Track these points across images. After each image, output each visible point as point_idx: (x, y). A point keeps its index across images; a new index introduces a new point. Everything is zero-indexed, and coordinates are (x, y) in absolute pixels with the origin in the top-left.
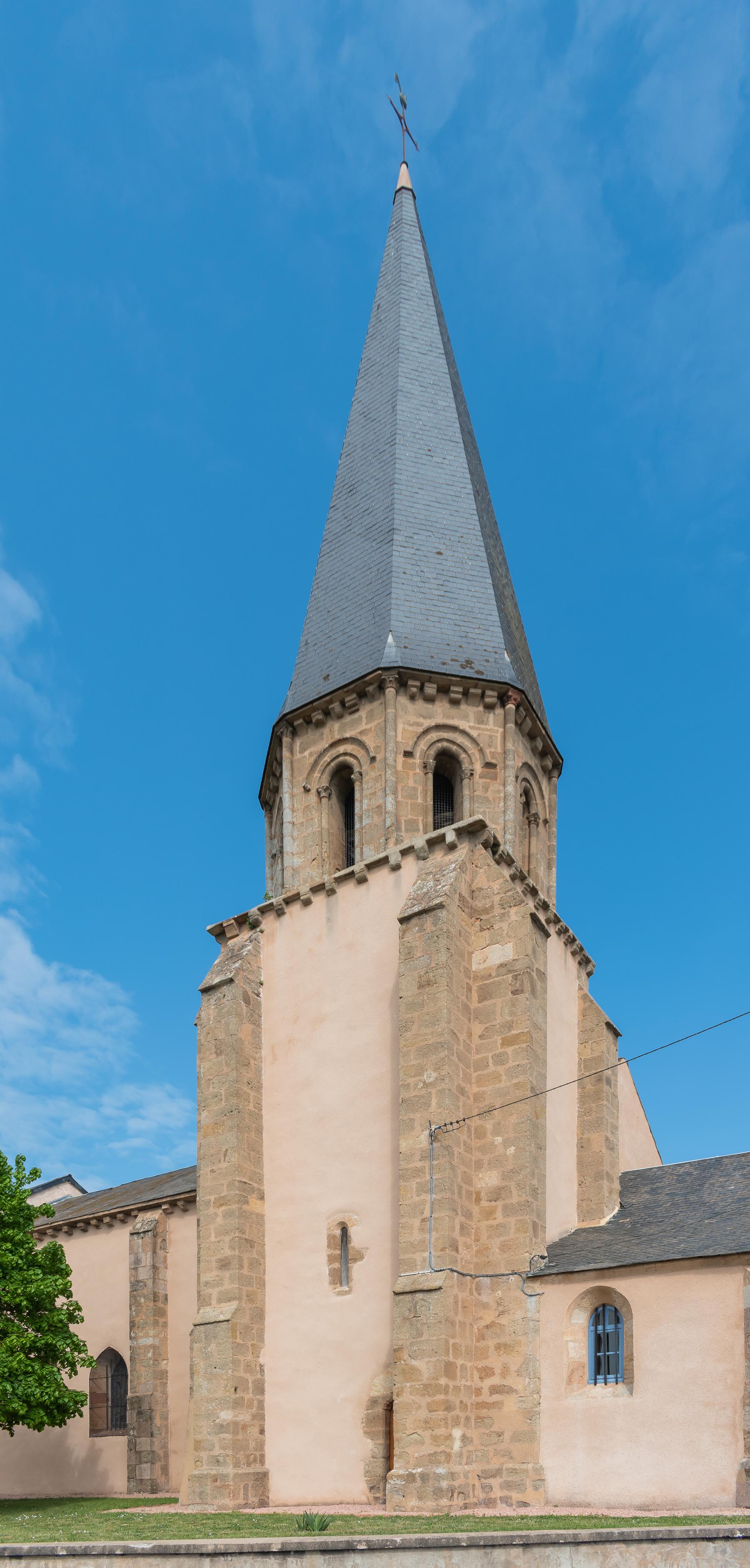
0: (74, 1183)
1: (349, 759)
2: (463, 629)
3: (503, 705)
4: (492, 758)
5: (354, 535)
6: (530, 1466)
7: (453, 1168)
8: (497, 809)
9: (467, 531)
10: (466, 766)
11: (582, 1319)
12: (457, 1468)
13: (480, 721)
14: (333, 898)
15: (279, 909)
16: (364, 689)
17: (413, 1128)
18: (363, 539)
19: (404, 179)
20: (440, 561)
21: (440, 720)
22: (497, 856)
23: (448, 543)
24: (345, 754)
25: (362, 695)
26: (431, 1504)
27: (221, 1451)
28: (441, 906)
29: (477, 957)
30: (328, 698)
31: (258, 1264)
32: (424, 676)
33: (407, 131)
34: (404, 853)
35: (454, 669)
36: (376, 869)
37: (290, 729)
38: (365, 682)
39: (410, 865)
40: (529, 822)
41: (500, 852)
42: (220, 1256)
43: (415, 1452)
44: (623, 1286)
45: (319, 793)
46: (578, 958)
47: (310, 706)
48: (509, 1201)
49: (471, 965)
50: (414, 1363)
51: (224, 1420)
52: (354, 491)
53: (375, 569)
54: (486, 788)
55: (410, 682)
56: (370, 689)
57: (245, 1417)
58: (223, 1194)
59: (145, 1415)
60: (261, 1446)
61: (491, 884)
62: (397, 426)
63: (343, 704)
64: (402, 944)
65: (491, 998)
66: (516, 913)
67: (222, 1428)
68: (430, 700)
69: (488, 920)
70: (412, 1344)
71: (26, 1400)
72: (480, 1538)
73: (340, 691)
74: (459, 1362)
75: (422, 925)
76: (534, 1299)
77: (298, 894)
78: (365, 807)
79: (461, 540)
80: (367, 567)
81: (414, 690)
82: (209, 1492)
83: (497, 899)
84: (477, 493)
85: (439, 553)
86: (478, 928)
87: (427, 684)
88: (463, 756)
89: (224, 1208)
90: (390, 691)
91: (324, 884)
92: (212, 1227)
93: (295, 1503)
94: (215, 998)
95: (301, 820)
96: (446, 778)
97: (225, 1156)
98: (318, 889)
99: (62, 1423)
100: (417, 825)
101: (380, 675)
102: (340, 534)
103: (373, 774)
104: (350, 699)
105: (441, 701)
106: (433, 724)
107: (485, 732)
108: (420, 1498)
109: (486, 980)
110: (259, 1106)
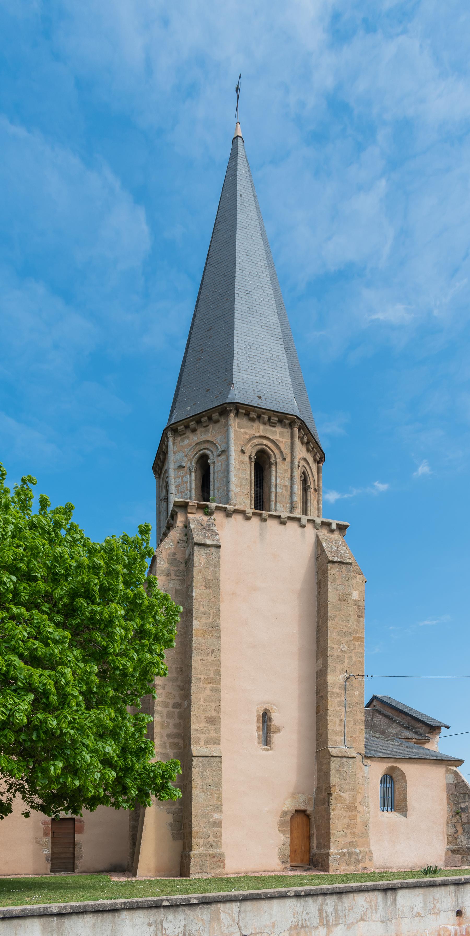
6: (367, 849)
14: (264, 524)
17: (335, 671)
26: (353, 867)
27: (214, 839)
30: (264, 411)
38: (286, 417)
42: (207, 715)
43: (342, 841)
44: (404, 767)
47: (253, 408)
48: (356, 718)
50: (342, 794)
51: (217, 819)
56: (287, 422)
58: (210, 677)
63: (269, 419)
70: (341, 784)
72: (302, 891)
76: (367, 767)
82: (208, 865)
89: (211, 685)
92: (202, 695)
93: (273, 870)
94: (205, 552)
97: (212, 653)
104: (274, 419)
108: (347, 865)
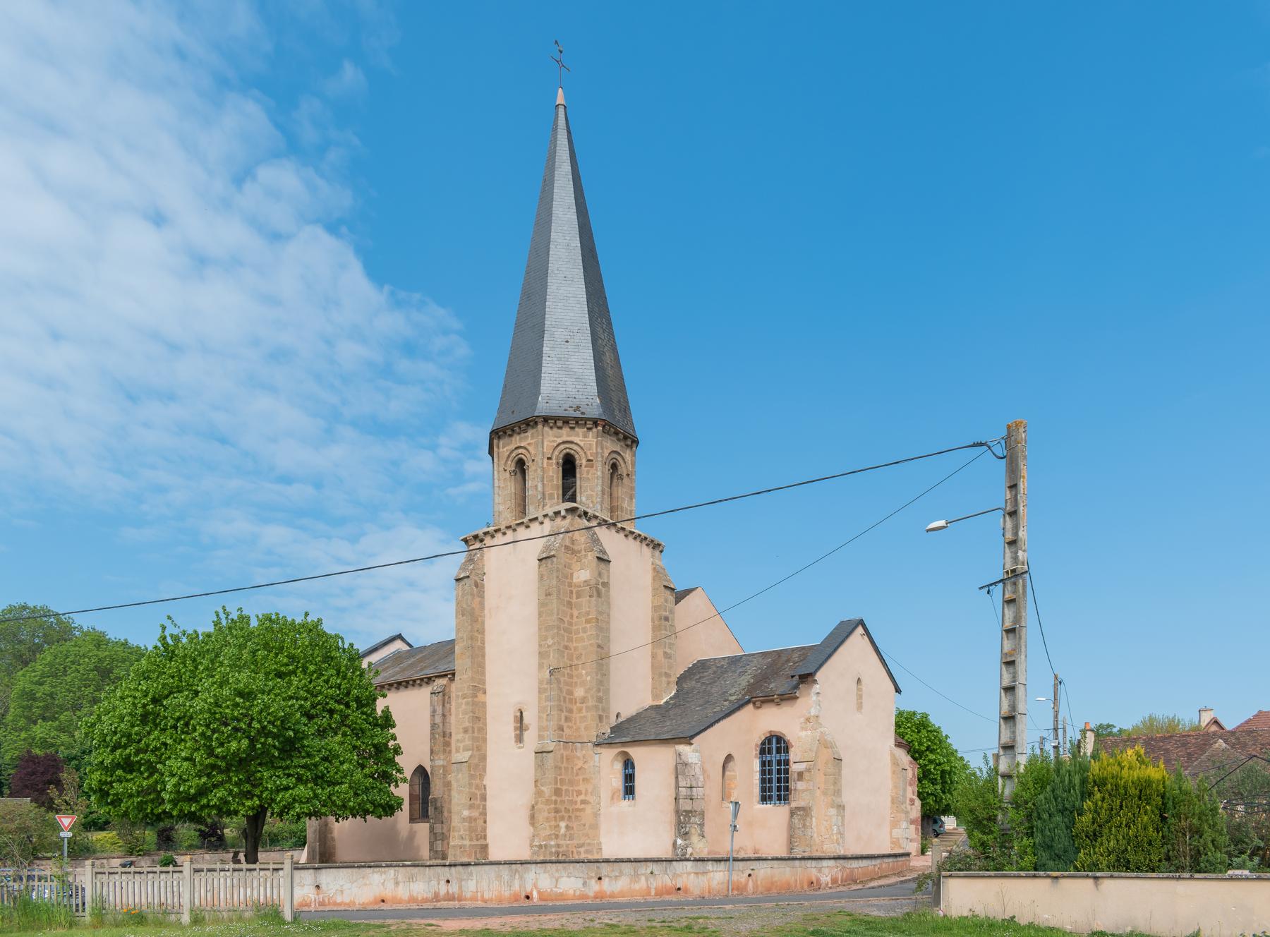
0: (403, 640)
7: (560, 689)
10: (577, 462)
11: (619, 766)
12: (562, 842)
13: (585, 436)
16: (529, 423)
21: (565, 438)
25: (528, 425)
31: (483, 730)
32: (556, 419)
34: (545, 516)
39: (547, 521)
54: (588, 472)
57: (475, 814)
59: (439, 810)
60: (484, 830)
67: (464, 820)
68: (560, 428)
71: (372, 803)
74: (564, 788)
90: (540, 426)
96: (569, 466)
98: (508, 527)
99: (392, 814)
107: (587, 444)
110: (483, 642)
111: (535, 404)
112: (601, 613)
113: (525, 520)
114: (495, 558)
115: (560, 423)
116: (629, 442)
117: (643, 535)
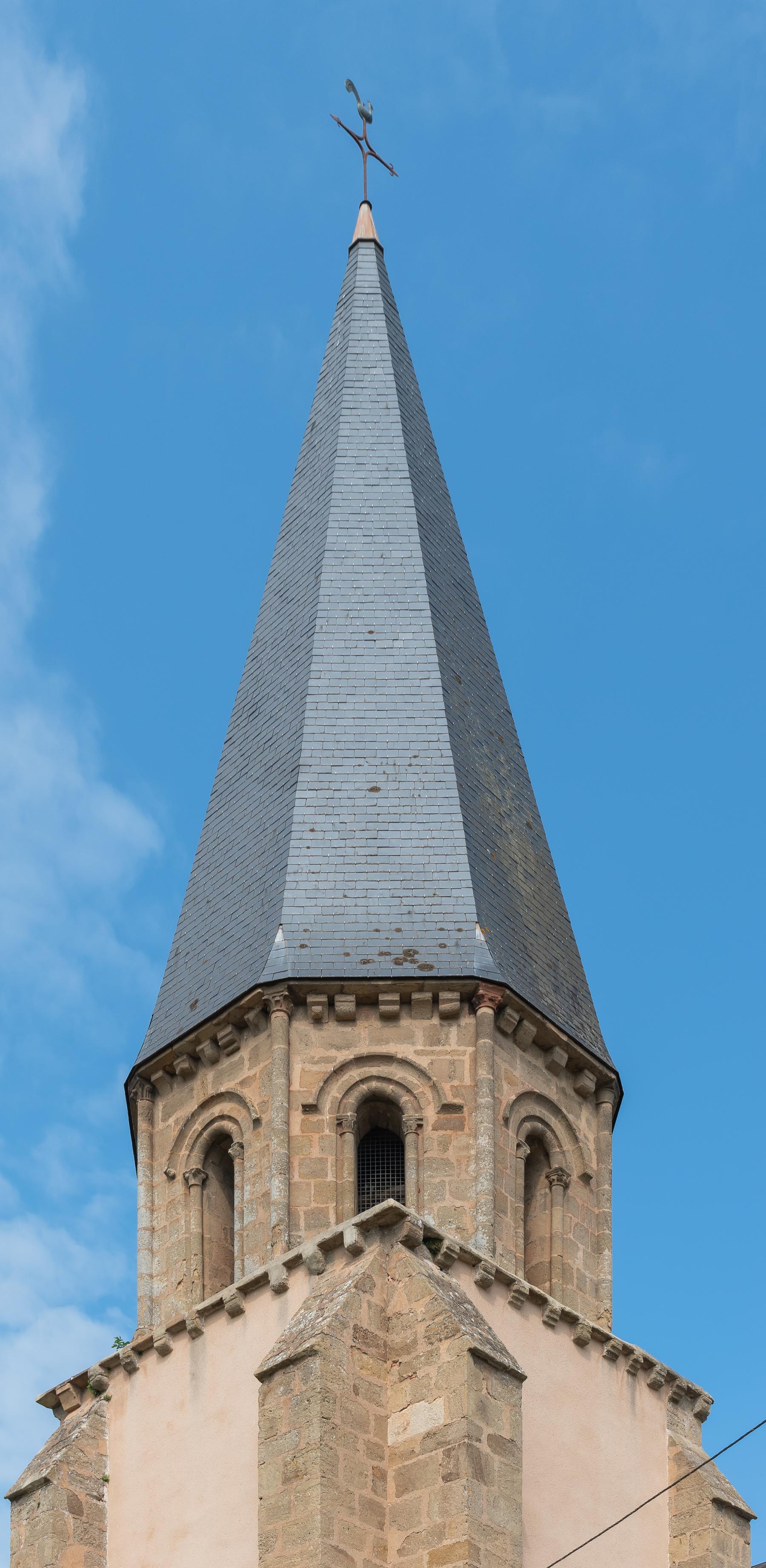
1: (227, 1125)
2: (405, 901)
3: (473, 1011)
4: (455, 1096)
5: (250, 780)
8: (464, 1176)
9: (425, 745)
10: (409, 1115)
14: (199, 1341)
15: (128, 1364)
16: (242, 1018)
18: (261, 785)
19: (365, 224)
20: (374, 802)
21: (364, 1049)
22: (439, 1257)
23: (390, 770)
24: (222, 1117)
25: (242, 1027)
28: (311, 1352)
29: (394, 1424)
33: (372, 153)
35: (386, 968)
36: (255, 1294)
37: (147, 1086)
38: (241, 1007)
39: (300, 1285)
40: (551, 1183)
41: (444, 1250)
45: (186, 1180)
46: (668, 1392)
49: (384, 1437)
52: (256, 713)
53: (270, 830)
54: (444, 1145)
55: (310, 999)
56: (250, 1016)
61: (414, 1305)
62: (320, 606)
63: (215, 1041)
64: (262, 1414)
65: (415, 1488)
66: (448, 1350)
68: (347, 1019)
69: (408, 1363)
73: (208, 1025)
75: (289, 1384)
77: (151, 1339)
78: (247, 1196)
79: (414, 761)
80: (261, 829)
81: (317, 1009)
83: (421, 1329)
84: (452, 683)
85: (375, 789)
86: (395, 1378)
87: (338, 998)
88: (405, 1099)
90: (278, 1018)
91: (183, 1322)
95: (163, 1223)
96: (380, 1142)
98: (177, 1329)
100: (326, 1216)
101: (262, 995)
102: (233, 781)
103: (258, 1145)
104: (225, 1033)
105: (367, 1018)
106: (352, 1057)
107: (446, 1064)
109: (407, 1459)
111: (264, 959)
112: (487, 1531)
113: (226, 1293)
114: (139, 1407)
115: (345, 1004)
116: (589, 1082)
117: (640, 1351)
